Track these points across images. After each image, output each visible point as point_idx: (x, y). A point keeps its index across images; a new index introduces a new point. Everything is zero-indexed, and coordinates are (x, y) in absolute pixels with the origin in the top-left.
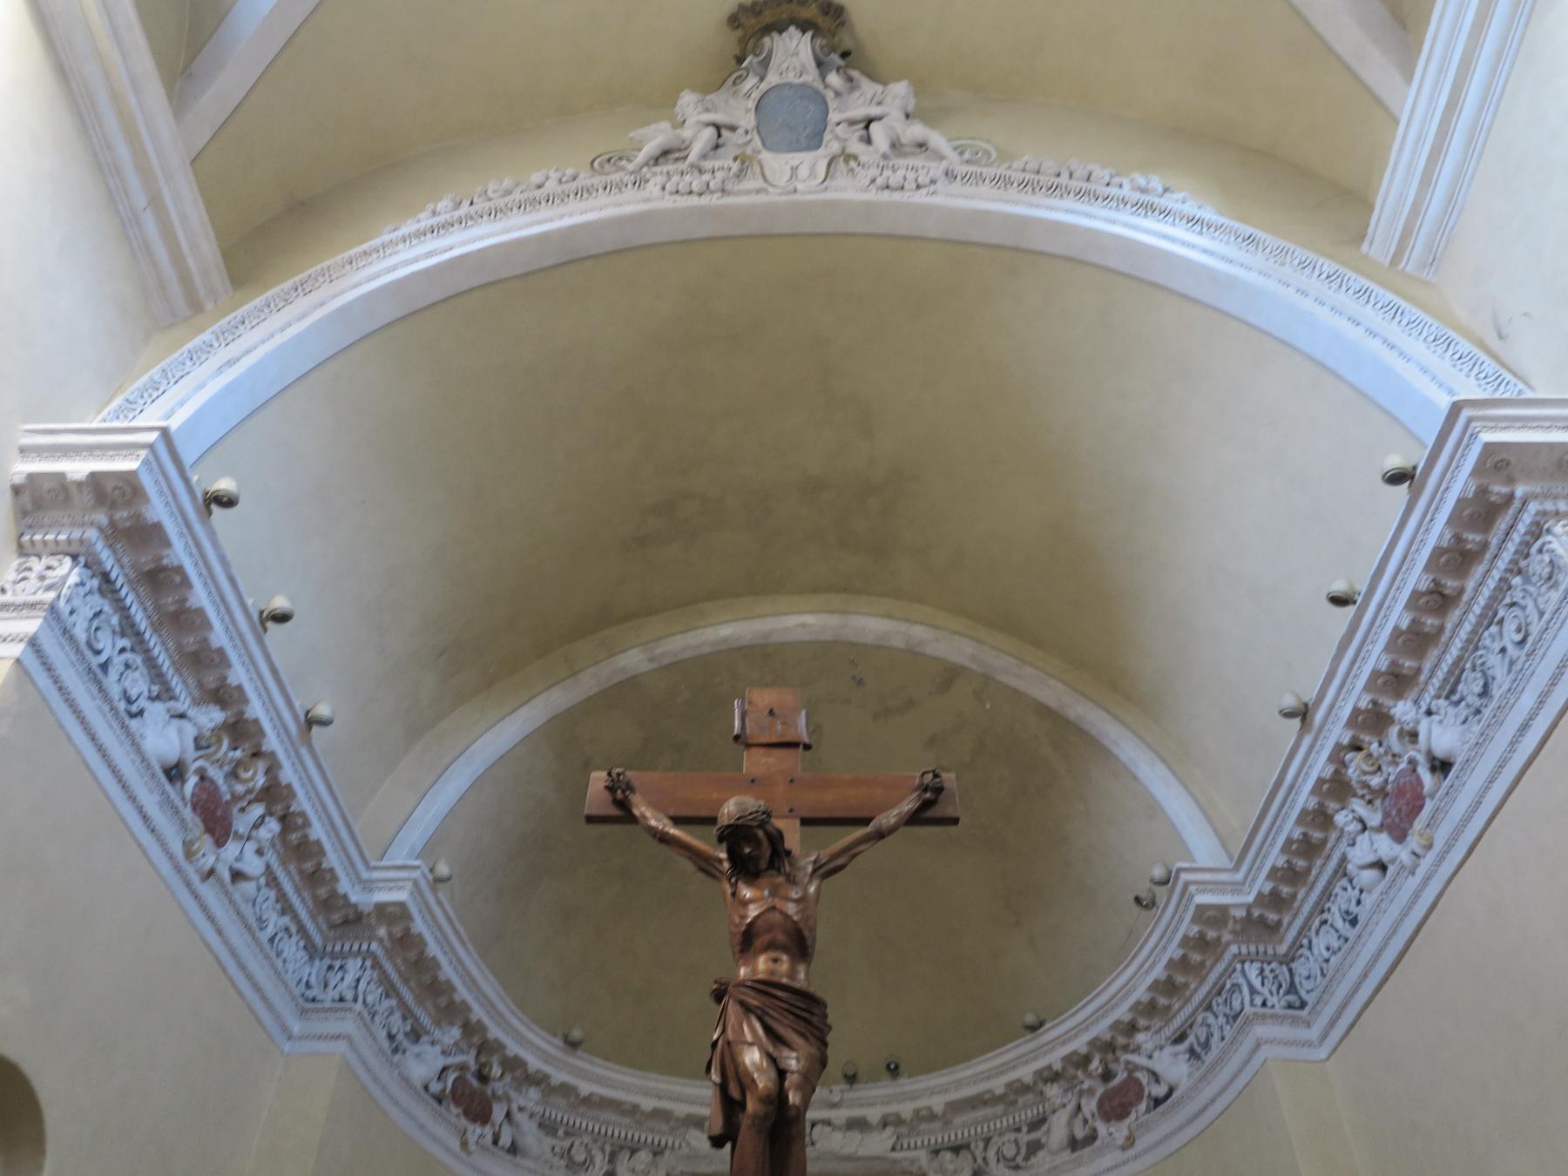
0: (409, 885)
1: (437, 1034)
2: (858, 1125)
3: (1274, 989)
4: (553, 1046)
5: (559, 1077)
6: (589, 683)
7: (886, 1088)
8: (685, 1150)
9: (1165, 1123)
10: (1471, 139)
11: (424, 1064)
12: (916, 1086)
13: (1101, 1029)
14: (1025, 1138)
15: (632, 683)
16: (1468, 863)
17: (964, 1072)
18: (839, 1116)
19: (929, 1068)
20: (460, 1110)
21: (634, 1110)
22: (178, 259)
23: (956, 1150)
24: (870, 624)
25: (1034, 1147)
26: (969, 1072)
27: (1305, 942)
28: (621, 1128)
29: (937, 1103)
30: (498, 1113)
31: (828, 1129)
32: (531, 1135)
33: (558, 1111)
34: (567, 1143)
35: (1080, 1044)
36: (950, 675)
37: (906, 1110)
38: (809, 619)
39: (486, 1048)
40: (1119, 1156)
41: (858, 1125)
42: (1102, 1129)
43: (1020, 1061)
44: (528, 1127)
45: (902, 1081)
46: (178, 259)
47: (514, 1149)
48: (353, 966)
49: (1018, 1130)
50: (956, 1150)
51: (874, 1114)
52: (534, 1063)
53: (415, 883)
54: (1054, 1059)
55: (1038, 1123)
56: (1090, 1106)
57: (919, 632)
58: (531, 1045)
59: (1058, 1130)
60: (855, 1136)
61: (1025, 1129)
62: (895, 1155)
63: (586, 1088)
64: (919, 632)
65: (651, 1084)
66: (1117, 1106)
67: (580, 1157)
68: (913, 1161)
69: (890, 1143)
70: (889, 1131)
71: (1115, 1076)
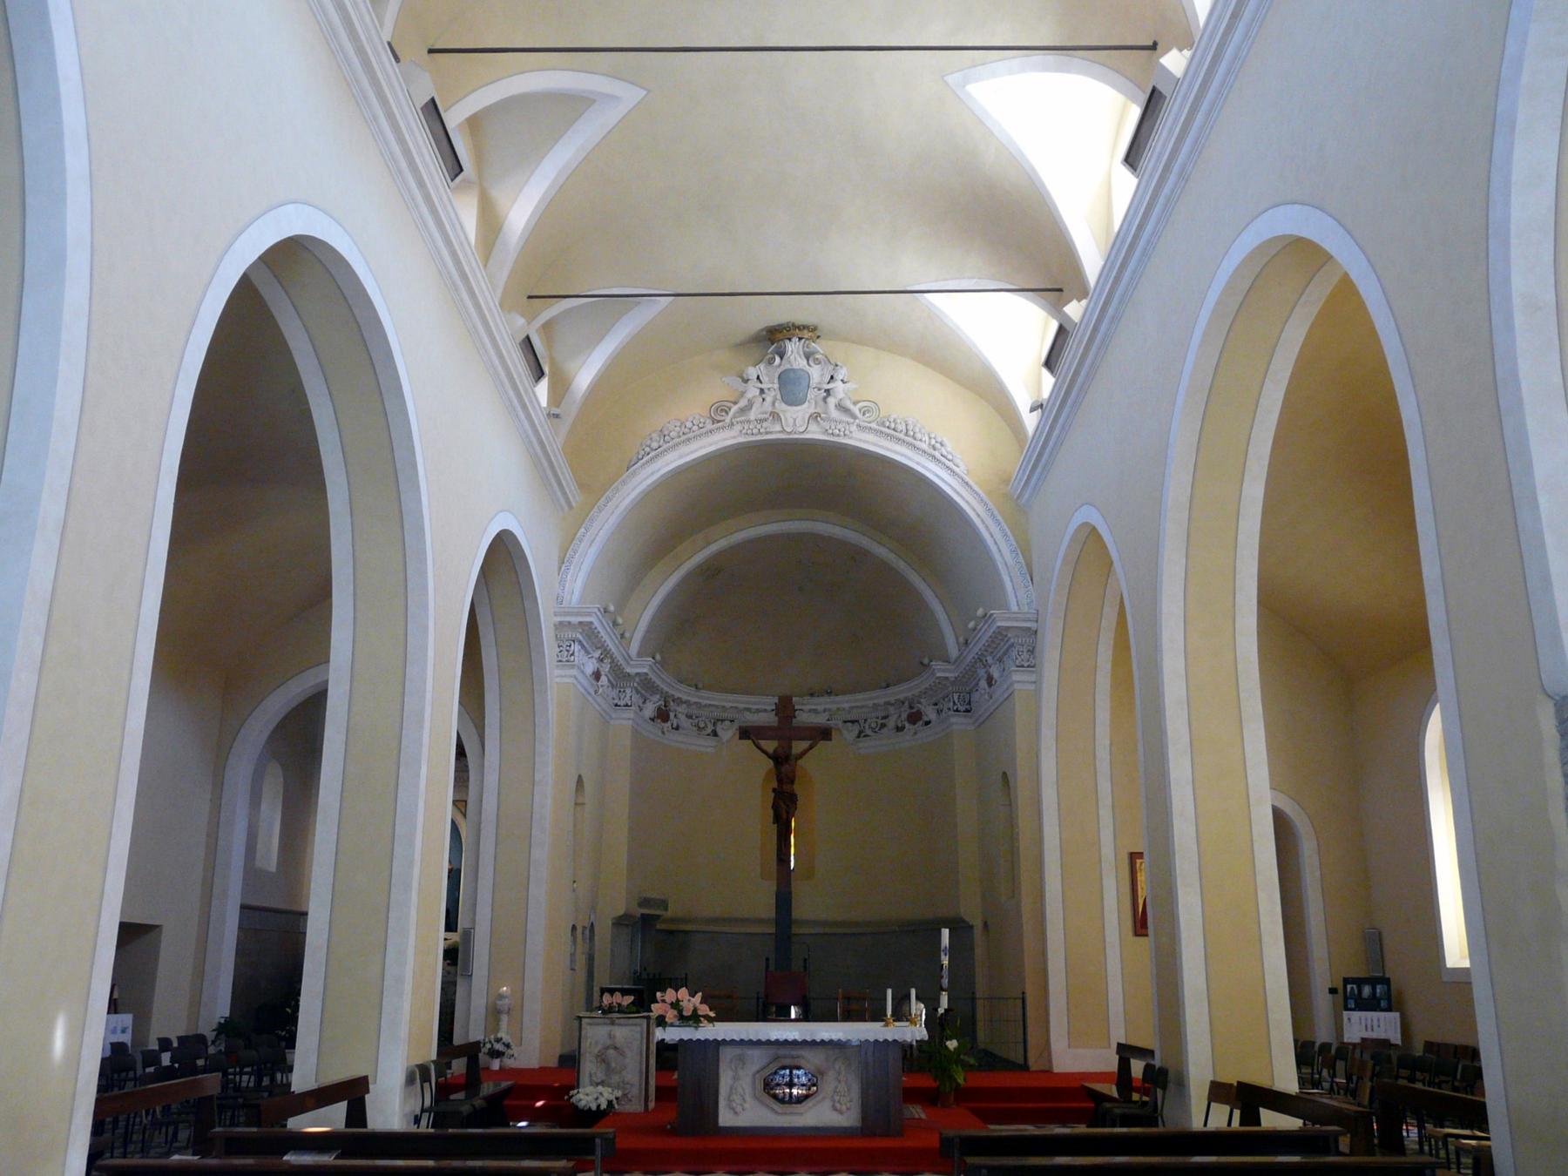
7: (826, 699)
10: (1063, 427)
11: (650, 710)
13: (909, 694)
16: (970, 44)
18: (807, 708)
25: (883, 726)
27: (982, 672)
29: (846, 706)
30: (672, 715)
35: (901, 697)
37: (834, 707)
39: (666, 698)
41: (815, 711)
44: (682, 717)
46: (541, 443)
48: (628, 691)
51: (820, 708)
52: (685, 698)
54: (892, 699)
56: (904, 716)
58: (683, 692)
59: (891, 723)
66: (915, 717)
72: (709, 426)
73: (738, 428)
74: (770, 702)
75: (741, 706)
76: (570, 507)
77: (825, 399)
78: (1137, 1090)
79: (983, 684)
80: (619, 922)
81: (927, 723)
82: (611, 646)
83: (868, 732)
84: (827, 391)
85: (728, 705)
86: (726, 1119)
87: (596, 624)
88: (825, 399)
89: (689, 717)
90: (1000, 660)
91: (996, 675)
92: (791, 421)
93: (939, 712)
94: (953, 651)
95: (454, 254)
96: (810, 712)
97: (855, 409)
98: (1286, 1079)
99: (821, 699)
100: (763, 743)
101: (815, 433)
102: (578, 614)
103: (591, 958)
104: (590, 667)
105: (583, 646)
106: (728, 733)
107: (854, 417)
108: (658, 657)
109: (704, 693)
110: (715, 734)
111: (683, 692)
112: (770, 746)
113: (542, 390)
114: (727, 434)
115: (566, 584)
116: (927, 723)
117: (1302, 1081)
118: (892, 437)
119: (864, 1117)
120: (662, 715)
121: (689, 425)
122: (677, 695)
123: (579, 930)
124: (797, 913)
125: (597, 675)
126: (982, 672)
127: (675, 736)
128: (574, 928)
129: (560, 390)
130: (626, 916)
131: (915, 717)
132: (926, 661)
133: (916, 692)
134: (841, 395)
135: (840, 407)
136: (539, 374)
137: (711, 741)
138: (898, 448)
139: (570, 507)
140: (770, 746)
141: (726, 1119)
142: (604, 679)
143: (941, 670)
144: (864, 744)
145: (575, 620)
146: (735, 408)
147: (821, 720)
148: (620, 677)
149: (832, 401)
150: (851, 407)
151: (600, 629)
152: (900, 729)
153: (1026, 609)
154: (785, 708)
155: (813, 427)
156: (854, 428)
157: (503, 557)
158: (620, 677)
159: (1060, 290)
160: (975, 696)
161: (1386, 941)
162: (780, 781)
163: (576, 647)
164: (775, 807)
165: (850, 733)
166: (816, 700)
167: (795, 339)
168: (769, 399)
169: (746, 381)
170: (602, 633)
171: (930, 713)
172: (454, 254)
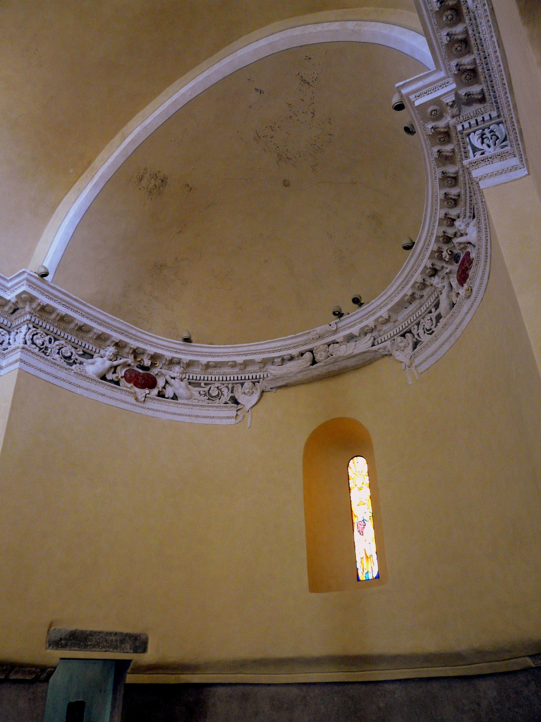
0: (25, 282)
1: (102, 352)
2: (350, 338)
3: (491, 143)
8: (270, 377)
12: (372, 307)
14: (434, 314)
19: (374, 296)
20: (132, 384)
21: (234, 365)
26: (393, 289)
28: (233, 374)
31: (336, 345)
34: (206, 389)
37: (370, 322)
40: (469, 302)
41: (350, 338)
45: (364, 307)
47: (175, 397)
49: (430, 312)
51: (355, 330)
53: (28, 280)
60: (352, 344)
61: (433, 310)
62: (374, 348)
67: (215, 393)
68: (385, 348)
69: (370, 343)
70: (369, 335)
71: (459, 257)
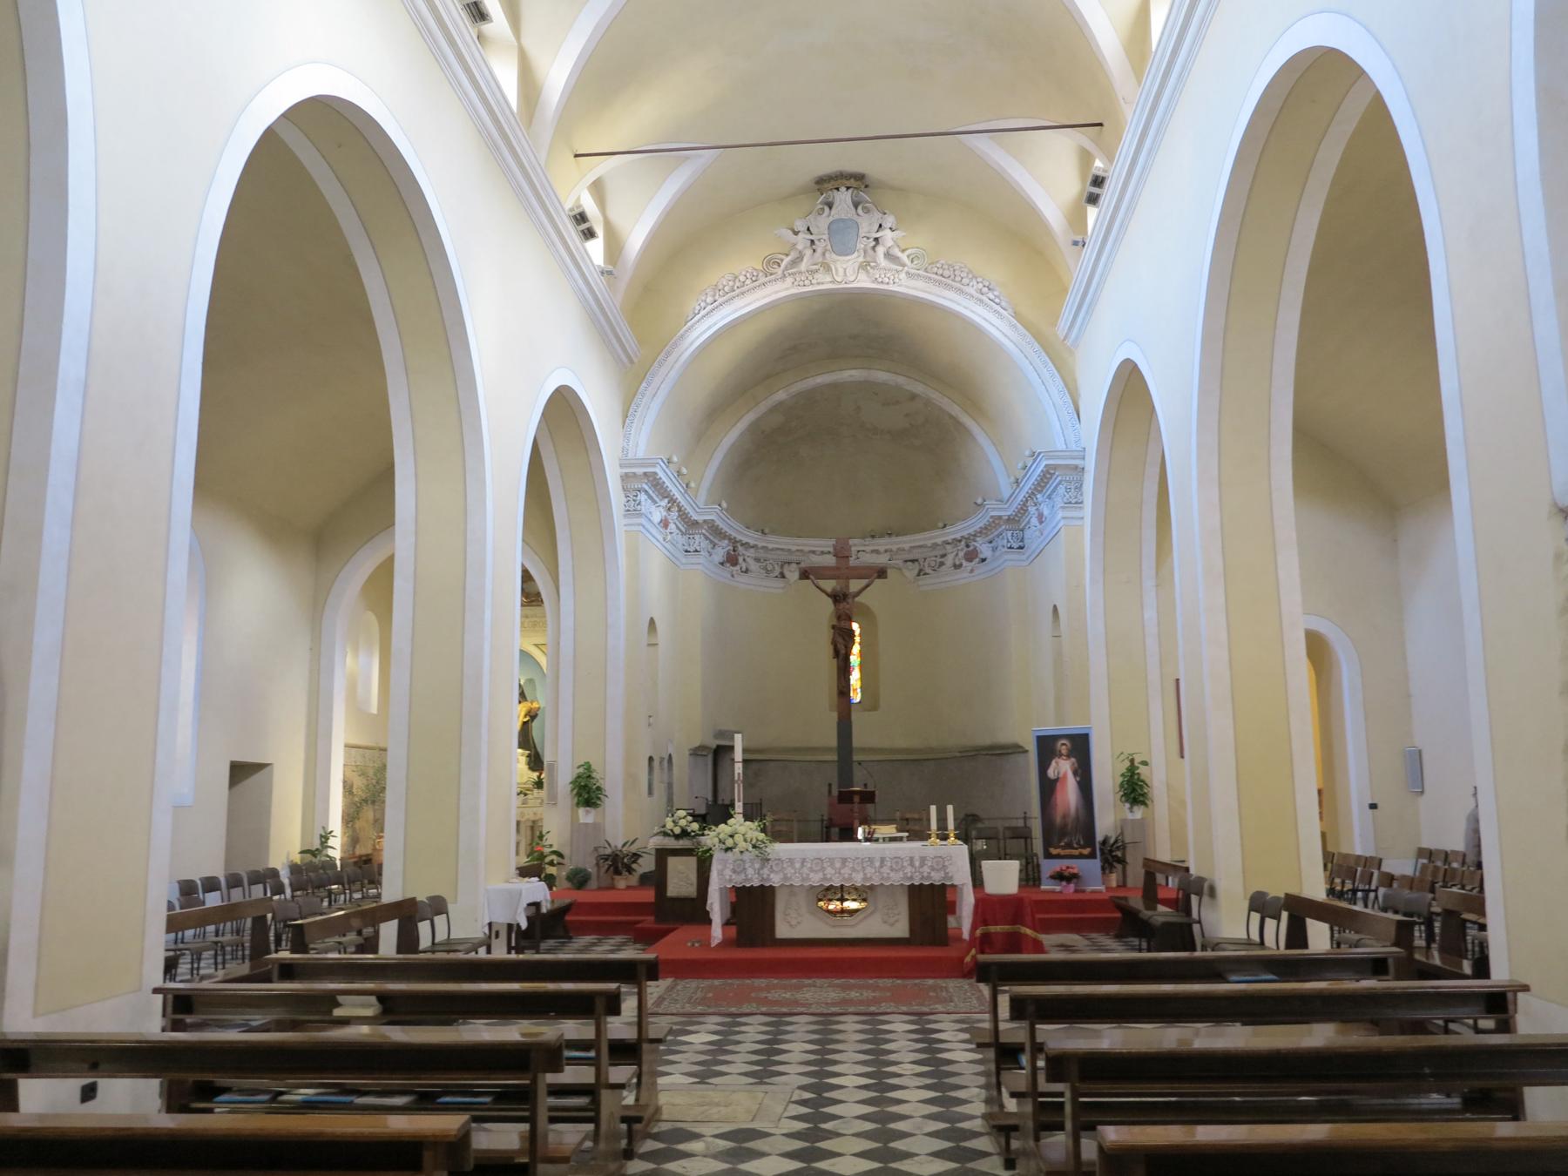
2: (877, 552)
4: (758, 535)
5: (760, 544)
6: (763, 407)
7: (886, 540)
9: (983, 568)
11: (719, 554)
13: (965, 533)
15: (781, 403)
17: (918, 536)
22: (625, 350)
23: (913, 561)
24: (881, 376)
25: (942, 564)
29: (907, 546)
32: (753, 566)
33: (761, 554)
35: (958, 536)
36: (913, 397)
37: (894, 548)
38: (853, 372)
41: (877, 552)
42: (965, 563)
43: (938, 536)
46: (625, 350)
47: (747, 571)
50: (913, 561)
51: (882, 549)
52: (752, 542)
54: (949, 538)
55: (943, 556)
56: (961, 554)
57: (901, 380)
58: (749, 537)
59: (949, 560)
63: (770, 546)
64: (901, 380)
65: (854, 994)
66: (971, 556)
72: (762, 279)
73: (789, 280)
74: (828, 544)
75: (807, 549)
76: (631, 361)
77: (874, 248)
78: (1166, 902)
79: (1034, 521)
80: (697, 752)
81: (983, 560)
82: (678, 496)
83: (928, 570)
84: (876, 239)
85: (794, 548)
86: (783, 931)
87: (661, 474)
88: (874, 248)
89: (757, 560)
90: (1049, 497)
91: (1046, 512)
92: (841, 271)
93: (994, 549)
94: (1006, 491)
95: (491, 112)
96: (866, 553)
97: (904, 257)
98: (1315, 888)
99: (882, 541)
100: (821, 583)
101: (864, 282)
102: (642, 465)
103: (670, 786)
104: (657, 515)
105: (650, 497)
106: (793, 575)
107: (904, 265)
108: (724, 505)
109: (772, 538)
110: (783, 576)
111: (749, 537)
112: (829, 585)
113: (596, 249)
114: (779, 286)
115: (623, 438)
116: (983, 560)
117: (1331, 892)
118: (940, 283)
119: (912, 931)
120: (732, 559)
121: (742, 278)
122: (745, 540)
123: (656, 763)
124: (858, 740)
125: (665, 523)
126: (1032, 509)
127: (744, 578)
128: (651, 759)
129: (614, 248)
130: (702, 747)
131: (971, 556)
132: (979, 501)
133: (971, 531)
134: (890, 243)
135: (888, 255)
136: (589, 234)
137: (780, 583)
138: (966, 302)
139: (631, 361)
140: (829, 585)
141: (783, 931)
142: (672, 526)
143: (994, 510)
144: (924, 581)
145: (640, 471)
146: (787, 260)
147: (882, 560)
148: (690, 525)
149: (881, 250)
150: (900, 254)
151: (664, 479)
152: (957, 567)
153: (1074, 447)
154: (841, 553)
155: (862, 276)
156: (903, 276)
157: (563, 411)
158: (690, 525)
159: (1101, 125)
160: (1027, 533)
161: (1425, 758)
162: (839, 618)
163: (642, 497)
164: (834, 643)
165: (910, 572)
166: (877, 541)
167: (843, 189)
168: (819, 251)
169: (796, 233)
170: (668, 483)
171: (985, 550)
172: (491, 112)
